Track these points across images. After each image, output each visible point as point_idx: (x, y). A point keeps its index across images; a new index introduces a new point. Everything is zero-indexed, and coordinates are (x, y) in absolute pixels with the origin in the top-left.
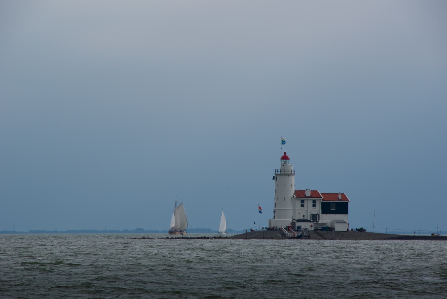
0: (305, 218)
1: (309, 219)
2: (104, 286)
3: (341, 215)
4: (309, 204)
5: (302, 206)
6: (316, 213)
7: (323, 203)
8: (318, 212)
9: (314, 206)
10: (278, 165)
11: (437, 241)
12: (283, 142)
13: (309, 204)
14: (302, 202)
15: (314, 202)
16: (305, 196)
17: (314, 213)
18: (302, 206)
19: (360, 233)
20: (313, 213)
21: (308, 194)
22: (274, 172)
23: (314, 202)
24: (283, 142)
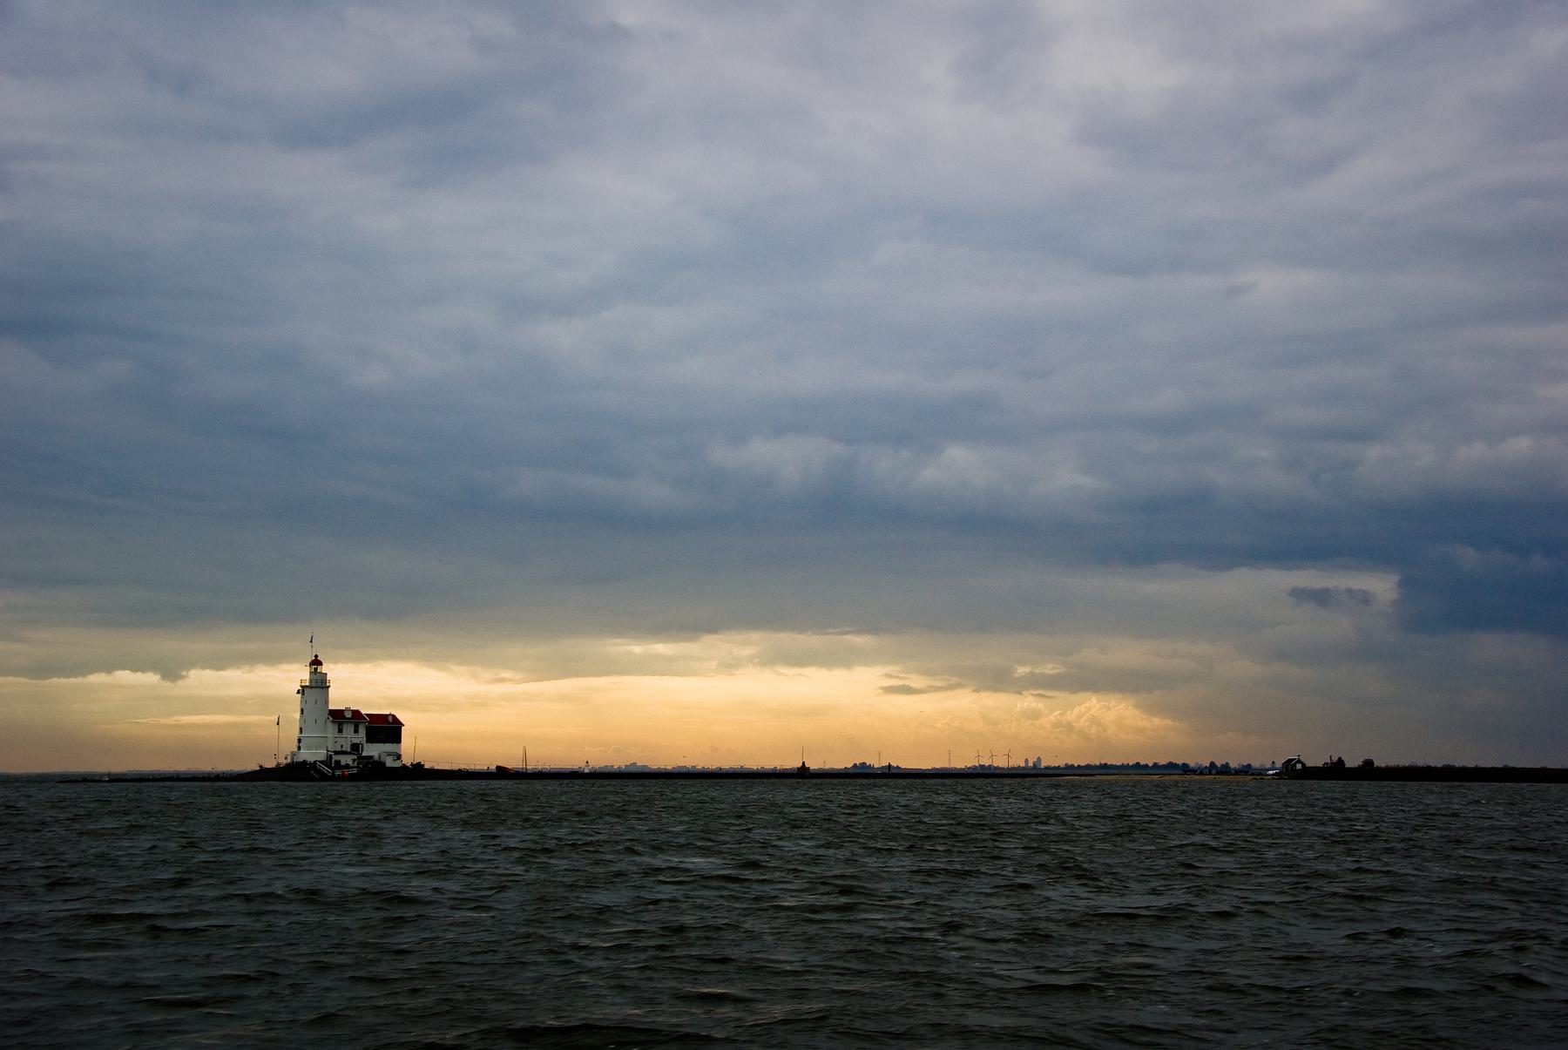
9: (356, 731)
19: (418, 771)
21: (348, 715)
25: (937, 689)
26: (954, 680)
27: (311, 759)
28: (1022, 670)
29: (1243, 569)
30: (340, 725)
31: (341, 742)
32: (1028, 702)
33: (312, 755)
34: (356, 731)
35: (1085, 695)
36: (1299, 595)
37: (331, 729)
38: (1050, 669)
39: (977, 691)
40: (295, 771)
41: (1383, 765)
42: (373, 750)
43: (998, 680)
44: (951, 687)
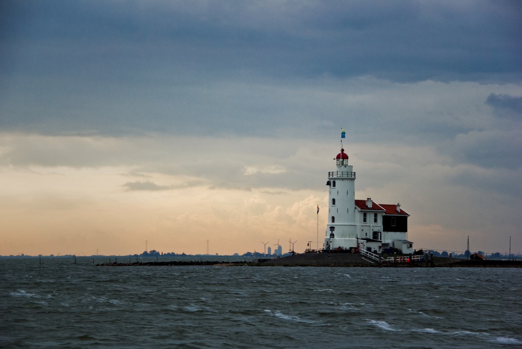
0: (368, 237)
1: (372, 238)
2: (485, 300)
3: (394, 233)
4: (370, 217)
5: (365, 220)
6: (377, 231)
7: (384, 218)
8: (379, 228)
9: (376, 221)
10: (333, 165)
11: (511, 269)
12: (343, 135)
13: (370, 217)
14: (365, 215)
15: (376, 216)
16: (367, 208)
17: (376, 230)
18: (365, 220)
19: (429, 260)
20: (374, 230)
21: (370, 205)
22: (328, 176)
23: (376, 216)
24: (343, 135)
25: (178, 187)
26: (193, 179)
27: (346, 246)
28: (251, 170)
29: (429, 82)
30: (365, 215)
31: (366, 230)
32: (254, 198)
33: (343, 241)
34: (376, 221)
35: (303, 192)
36: (492, 100)
37: (359, 216)
38: (274, 170)
39: (213, 188)
40: (330, 257)
41: (242, 254)
42: (389, 238)
43: (230, 179)
44: (192, 184)
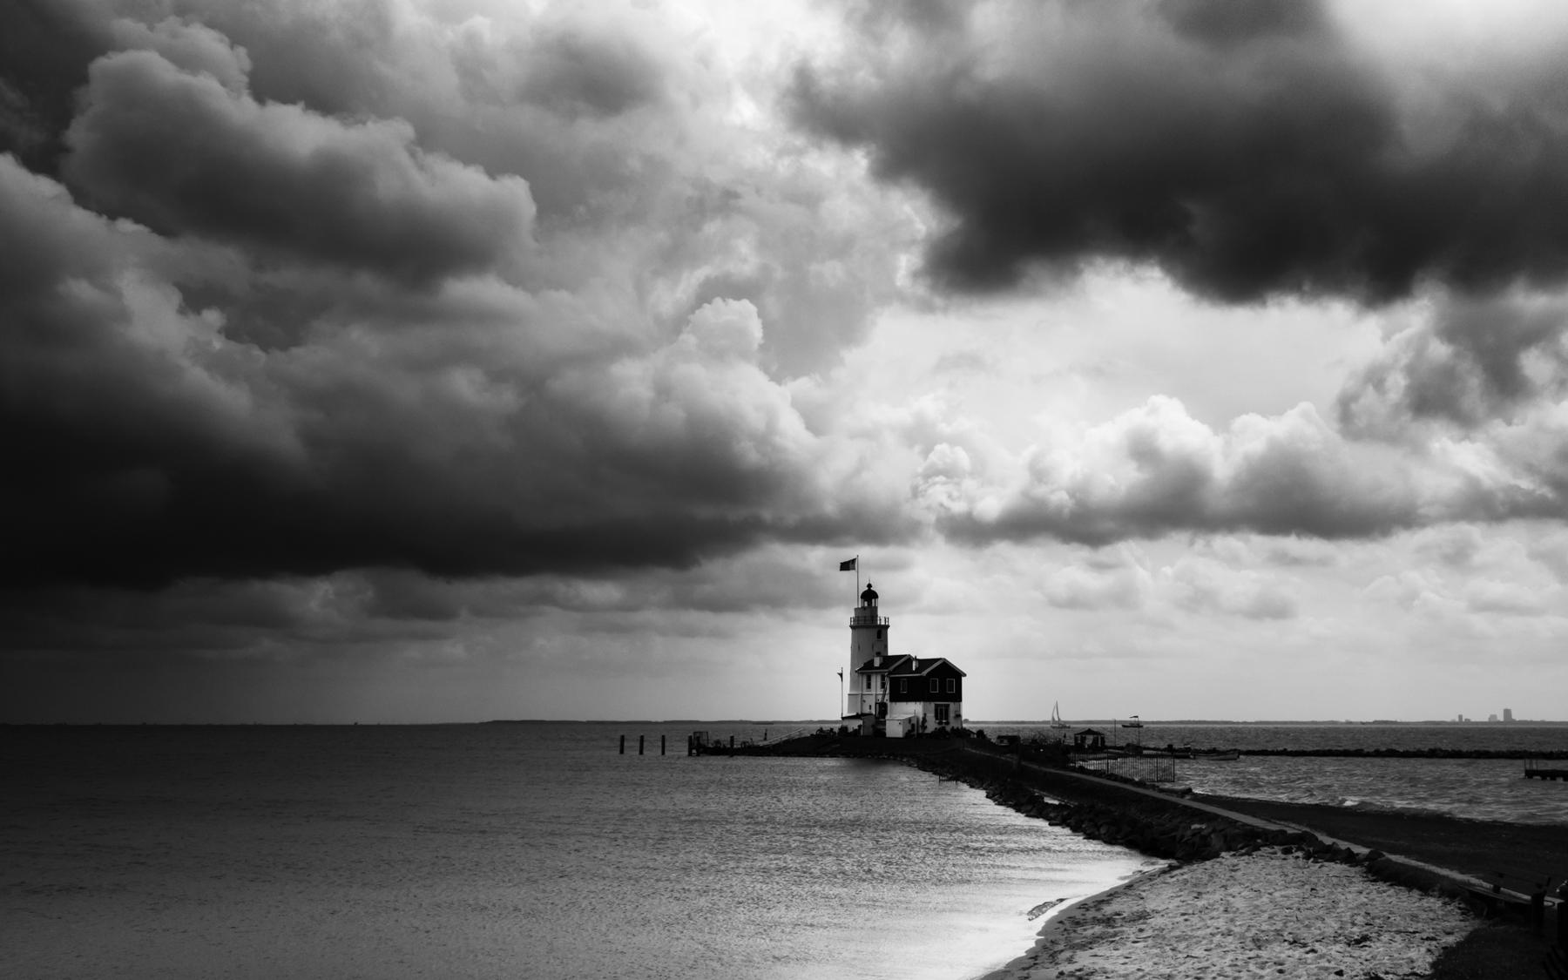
9: (883, 686)
